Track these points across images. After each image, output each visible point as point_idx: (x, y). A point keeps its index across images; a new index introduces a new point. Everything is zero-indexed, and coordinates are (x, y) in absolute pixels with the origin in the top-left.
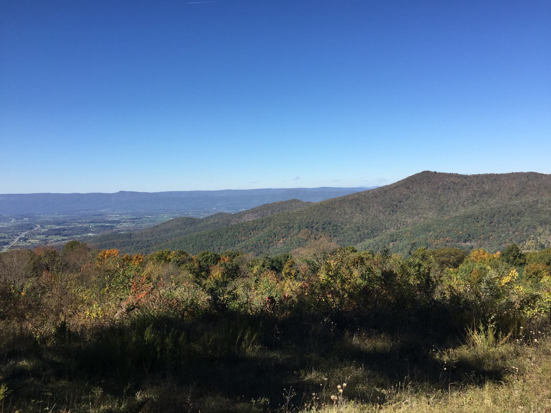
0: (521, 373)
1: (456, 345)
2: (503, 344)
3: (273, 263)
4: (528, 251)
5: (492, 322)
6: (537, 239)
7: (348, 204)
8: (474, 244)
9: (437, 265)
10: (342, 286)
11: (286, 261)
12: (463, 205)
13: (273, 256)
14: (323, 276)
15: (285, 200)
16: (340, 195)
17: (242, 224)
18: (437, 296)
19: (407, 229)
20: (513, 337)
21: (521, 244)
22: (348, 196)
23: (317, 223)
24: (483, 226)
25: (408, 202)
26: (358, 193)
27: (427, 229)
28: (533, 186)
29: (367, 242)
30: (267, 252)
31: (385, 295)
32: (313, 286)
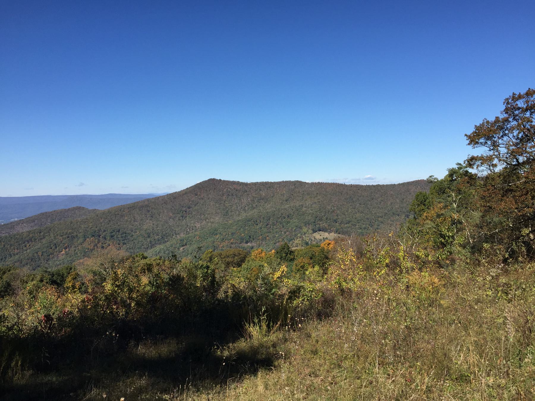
0: (287, 357)
1: (235, 340)
2: (274, 333)
3: (52, 277)
4: (296, 248)
5: (264, 314)
6: (302, 238)
7: (138, 210)
8: (254, 244)
9: (223, 266)
10: (129, 295)
11: (69, 273)
12: (244, 210)
13: (54, 269)
14: (108, 287)
15: (67, 208)
16: (129, 202)
17: (14, 236)
18: (221, 295)
19: (196, 233)
20: (282, 325)
21: (291, 243)
22: (138, 202)
23: (105, 231)
24: (261, 228)
25: (196, 208)
26: (148, 200)
27: (214, 232)
28: (299, 192)
29: (158, 248)
30: (47, 265)
31: (173, 300)
32: (96, 298)
